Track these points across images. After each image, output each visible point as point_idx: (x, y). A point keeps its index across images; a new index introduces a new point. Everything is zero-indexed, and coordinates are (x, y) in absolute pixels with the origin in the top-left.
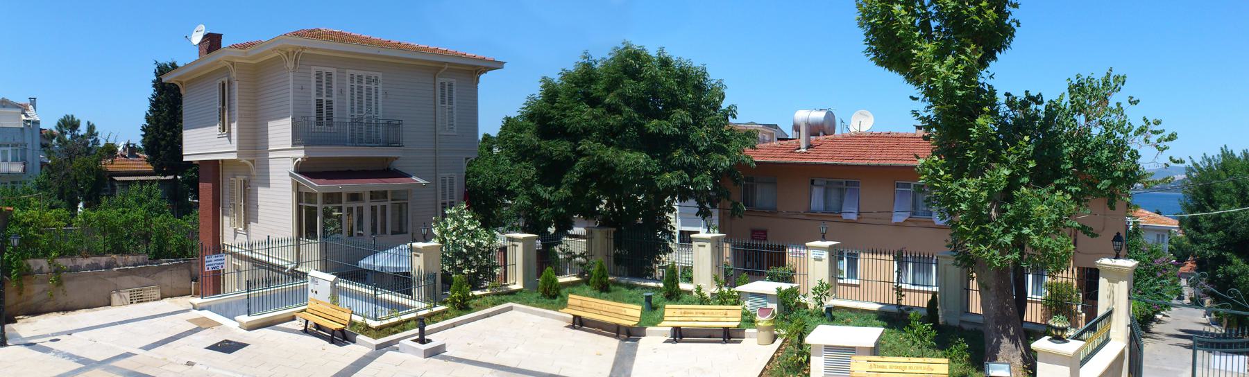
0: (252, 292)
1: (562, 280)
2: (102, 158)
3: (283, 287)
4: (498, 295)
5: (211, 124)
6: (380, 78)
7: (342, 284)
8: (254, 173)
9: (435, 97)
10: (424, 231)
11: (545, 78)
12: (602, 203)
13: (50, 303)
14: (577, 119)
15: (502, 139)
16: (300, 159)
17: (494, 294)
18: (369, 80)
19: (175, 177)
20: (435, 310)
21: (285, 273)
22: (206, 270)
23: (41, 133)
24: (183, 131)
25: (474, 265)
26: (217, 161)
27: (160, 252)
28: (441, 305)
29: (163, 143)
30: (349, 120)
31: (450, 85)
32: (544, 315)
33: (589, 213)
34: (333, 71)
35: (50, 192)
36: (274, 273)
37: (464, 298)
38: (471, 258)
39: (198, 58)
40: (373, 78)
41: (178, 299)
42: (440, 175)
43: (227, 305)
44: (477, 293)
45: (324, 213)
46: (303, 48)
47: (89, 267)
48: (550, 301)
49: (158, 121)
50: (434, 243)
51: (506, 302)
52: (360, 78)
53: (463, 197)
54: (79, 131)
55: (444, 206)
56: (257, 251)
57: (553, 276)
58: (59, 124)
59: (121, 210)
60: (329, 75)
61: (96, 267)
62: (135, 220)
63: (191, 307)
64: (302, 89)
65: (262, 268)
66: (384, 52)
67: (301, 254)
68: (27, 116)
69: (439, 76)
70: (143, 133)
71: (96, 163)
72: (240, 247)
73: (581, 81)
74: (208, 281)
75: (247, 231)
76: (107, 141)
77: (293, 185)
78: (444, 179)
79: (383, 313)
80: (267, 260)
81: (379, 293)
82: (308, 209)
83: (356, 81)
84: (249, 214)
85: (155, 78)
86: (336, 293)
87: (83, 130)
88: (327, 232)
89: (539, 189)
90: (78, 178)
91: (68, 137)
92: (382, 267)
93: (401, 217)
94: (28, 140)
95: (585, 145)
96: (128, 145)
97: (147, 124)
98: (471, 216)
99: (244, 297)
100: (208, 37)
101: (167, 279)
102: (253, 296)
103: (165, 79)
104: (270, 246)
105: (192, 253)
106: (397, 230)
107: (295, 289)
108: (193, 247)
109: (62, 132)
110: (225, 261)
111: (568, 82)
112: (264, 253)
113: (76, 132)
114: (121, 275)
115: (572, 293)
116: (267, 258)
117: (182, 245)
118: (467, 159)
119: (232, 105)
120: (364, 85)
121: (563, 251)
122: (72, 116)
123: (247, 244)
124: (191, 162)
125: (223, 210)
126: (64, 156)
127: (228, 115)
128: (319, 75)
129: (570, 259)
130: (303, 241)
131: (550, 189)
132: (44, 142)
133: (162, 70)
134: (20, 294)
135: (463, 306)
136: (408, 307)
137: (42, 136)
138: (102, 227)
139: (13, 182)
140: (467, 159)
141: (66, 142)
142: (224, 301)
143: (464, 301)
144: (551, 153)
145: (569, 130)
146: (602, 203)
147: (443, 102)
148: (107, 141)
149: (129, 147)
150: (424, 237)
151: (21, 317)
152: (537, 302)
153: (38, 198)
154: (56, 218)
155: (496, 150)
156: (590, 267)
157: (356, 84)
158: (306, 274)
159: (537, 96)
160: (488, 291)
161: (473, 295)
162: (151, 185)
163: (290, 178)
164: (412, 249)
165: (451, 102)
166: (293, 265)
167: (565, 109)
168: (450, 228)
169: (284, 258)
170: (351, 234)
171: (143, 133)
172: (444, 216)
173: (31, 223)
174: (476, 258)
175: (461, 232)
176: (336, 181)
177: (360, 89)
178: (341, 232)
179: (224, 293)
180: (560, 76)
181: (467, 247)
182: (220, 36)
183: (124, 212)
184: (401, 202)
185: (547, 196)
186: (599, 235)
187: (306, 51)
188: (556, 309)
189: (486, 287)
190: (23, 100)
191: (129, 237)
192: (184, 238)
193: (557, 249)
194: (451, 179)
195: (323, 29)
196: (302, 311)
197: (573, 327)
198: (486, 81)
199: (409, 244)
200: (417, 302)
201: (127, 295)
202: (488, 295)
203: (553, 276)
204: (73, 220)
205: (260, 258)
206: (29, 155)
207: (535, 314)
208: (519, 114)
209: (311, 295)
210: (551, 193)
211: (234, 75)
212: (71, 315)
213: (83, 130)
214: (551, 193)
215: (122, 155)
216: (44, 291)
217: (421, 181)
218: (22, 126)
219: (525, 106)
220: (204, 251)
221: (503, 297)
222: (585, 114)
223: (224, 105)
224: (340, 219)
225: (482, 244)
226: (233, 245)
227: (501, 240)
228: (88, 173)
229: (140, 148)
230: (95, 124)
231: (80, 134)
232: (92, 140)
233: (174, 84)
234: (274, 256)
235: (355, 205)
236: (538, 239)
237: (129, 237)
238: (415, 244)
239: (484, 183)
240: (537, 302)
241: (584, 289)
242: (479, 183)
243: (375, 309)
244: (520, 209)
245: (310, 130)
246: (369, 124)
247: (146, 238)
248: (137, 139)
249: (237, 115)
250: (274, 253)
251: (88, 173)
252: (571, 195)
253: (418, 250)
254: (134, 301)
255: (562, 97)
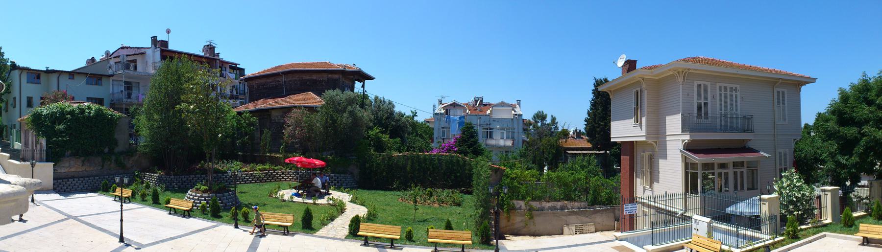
0: (655, 230)
1: (855, 215)
2: (560, 138)
3: (676, 227)
4: (816, 227)
5: (630, 118)
6: (739, 88)
7: (715, 224)
8: (657, 150)
9: (774, 101)
10: (768, 187)
11: (841, 88)
12: (877, 165)
13: (525, 230)
14: (861, 113)
15: (816, 126)
16: (687, 141)
17: (814, 227)
18: (731, 89)
19: (606, 152)
20: (777, 240)
21: (677, 217)
22: (625, 214)
23: (523, 122)
24: (611, 122)
25: (801, 209)
26: (632, 142)
27: (595, 200)
28: (780, 236)
29: (598, 129)
30: (718, 116)
31: (783, 93)
32: (845, 238)
33: (870, 172)
34: (708, 84)
35: (527, 159)
36: (670, 216)
37: (795, 231)
38: (798, 204)
39: (621, 75)
40: (734, 88)
41: (606, 233)
42: (778, 151)
43: (639, 238)
44: (803, 227)
45: (702, 177)
46: (689, 69)
47: (550, 208)
48: (849, 229)
49: (595, 115)
50: (775, 195)
51: (822, 232)
52: (725, 89)
53: (792, 165)
54: (546, 121)
55: (781, 171)
56: (658, 202)
57: (850, 213)
58: (534, 117)
59: (570, 172)
60: (706, 86)
61: (554, 208)
62: (579, 179)
63: (615, 238)
64: (688, 95)
65: (662, 213)
66: (740, 72)
67: (688, 204)
68: (515, 111)
69: (776, 87)
70: (586, 123)
71: (556, 141)
72: (647, 199)
73: (862, 90)
74: (626, 221)
75: (652, 189)
76: (563, 127)
77: (682, 157)
78: (780, 153)
79: (742, 244)
80: (665, 208)
81: (740, 230)
82: (692, 174)
83: (723, 90)
84: (654, 178)
85: (594, 88)
86: (711, 230)
87: (548, 120)
88: (705, 189)
89: (840, 158)
90: (545, 150)
91: (539, 124)
92: (741, 212)
93: (753, 178)
94: (516, 126)
95: (866, 129)
96: (576, 130)
97: (589, 118)
98: (798, 177)
99: (649, 233)
100: (627, 62)
101: (599, 219)
102: (655, 232)
103: (600, 89)
104: (667, 199)
105: (616, 202)
106: (751, 187)
107: (683, 228)
108: (616, 198)
109: (536, 122)
110: (637, 208)
111: (855, 91)
112: (663, 203)
113: (544, 122)
114: (569, 215)
115: (861, 223)
116: (665, 206)
117: (609, 197)
118: (794, 140)
119: (643, 106)
120: (728, 93)
121: (855, 196)
122: (542, 112)
123: (652, 197)
124: (616, 142)
125: (636, 174)
126: (536, 137)
127: (640, 112)
128: (699, 86)
129: (859, 201)
130: (689, 195)
131: (846, 157)
132: (525, 127)
133: (598, 83)
134: (509, 221)
135: (795, 237)
136: (759, 239)
137: (524, 124)
138: (559, 183)
139: (506, 152)
140: (794, 140)
141: (538, 128)
142: (636, 235)
143: (795, 232)
144: (846, 135)
145: (856, 120)
146: (877, 165)
147: (779, 103)
148: (563, 127)
149: (577, 132)
150: (769, 192)
151: (508, 235)
152: (841, 230)
153: (520, 162)
154: (531, 175)
155: (812, 134)
156: (871, 205)
157: (723, 92)
158: (691, 217)
159: (836, 99)
160: (810, 225)
161: (800, 229)
162: (590, 156)
163: (680, 154)
164: (760, 199)
165: (784, 104)
166: (682, 212)
167: (854, 107)
168: (785, 185)
169: (676, 207)
170: (720, 190)
171: (586, 123)
172: (781, 177)
173: (516, 177)
174: (802, 204)
175: (792, 187)
176: (711, 155)
177: (726, 95)
178: (714, 189)
179: (636, 229)
180: (850, 87)
181: (796, 197)
182: (635, 62)
183: (573, 174)
184: (753, 169)
185: (844, 162)
186: (876, 184)
187: (690, 71)
188: (852, 234)
189: (809, 223)
190: (514, 102)
191: (575, 190)
192: (611, 192)
193: (852, 195)
194: (785, 153)
195: (702, 57)
196: (688, 243)
197: (863, 244)
198: (806, 91)
199: (759, 197)
200: (764, 235)
201: (573, 228)
202: (810, 228)
203: (850, 213)
204: (541, 177)
205: (661, 207)
206: (516, 135)
207: (839, 238)
208: (826, 111)
209: (694, 232)
210: (847, 160)
211: (644, 86)
212: (538, 239)
213: (548, 120)
214: (847, 160)
215: (572, 137)
216: (522, 221)
217: (766, 155)
218: (512, 118)
219: (830, 106)
220: (623, 201)
221: (820, 229)
222: (865, 111)
223: (637, 105)
224: (713, 180)
225: (805, 195)
226: (643, 197)
227: (817, 191)
228: (551, 148)
229: (584, 133)
230: (556, 117)
231: (547, 123)
232: (554, 127)
233: (606, 92)
234: (669, 205)
235: (723, 171)
236: (840, 190)
237: (575, 190)
238: (762, 197)
239: (806, 155)
240: (841, 230)
241: (869, 219)
242: (803, 155)
243: (737, 241)
244: (828, 171)
245: (693, 122)
246: (732, 118)
247: (586, 191)
248: (582, 127)
249: (646, 113)
250: (670, 203)
251: (551, 148)
252: (859, 161)
253: (764, 200)
254: (578, 233)
255: (851, 100)
